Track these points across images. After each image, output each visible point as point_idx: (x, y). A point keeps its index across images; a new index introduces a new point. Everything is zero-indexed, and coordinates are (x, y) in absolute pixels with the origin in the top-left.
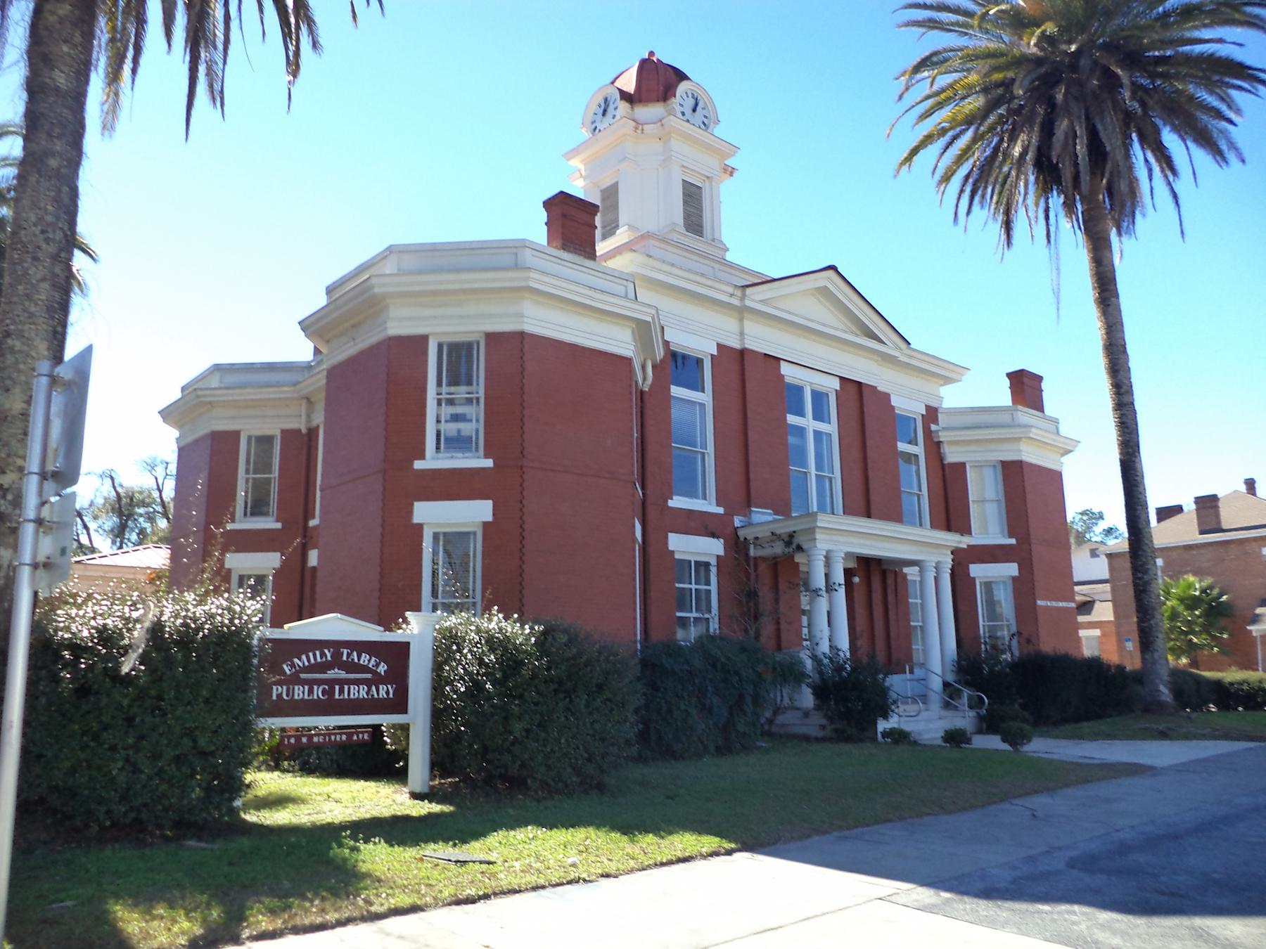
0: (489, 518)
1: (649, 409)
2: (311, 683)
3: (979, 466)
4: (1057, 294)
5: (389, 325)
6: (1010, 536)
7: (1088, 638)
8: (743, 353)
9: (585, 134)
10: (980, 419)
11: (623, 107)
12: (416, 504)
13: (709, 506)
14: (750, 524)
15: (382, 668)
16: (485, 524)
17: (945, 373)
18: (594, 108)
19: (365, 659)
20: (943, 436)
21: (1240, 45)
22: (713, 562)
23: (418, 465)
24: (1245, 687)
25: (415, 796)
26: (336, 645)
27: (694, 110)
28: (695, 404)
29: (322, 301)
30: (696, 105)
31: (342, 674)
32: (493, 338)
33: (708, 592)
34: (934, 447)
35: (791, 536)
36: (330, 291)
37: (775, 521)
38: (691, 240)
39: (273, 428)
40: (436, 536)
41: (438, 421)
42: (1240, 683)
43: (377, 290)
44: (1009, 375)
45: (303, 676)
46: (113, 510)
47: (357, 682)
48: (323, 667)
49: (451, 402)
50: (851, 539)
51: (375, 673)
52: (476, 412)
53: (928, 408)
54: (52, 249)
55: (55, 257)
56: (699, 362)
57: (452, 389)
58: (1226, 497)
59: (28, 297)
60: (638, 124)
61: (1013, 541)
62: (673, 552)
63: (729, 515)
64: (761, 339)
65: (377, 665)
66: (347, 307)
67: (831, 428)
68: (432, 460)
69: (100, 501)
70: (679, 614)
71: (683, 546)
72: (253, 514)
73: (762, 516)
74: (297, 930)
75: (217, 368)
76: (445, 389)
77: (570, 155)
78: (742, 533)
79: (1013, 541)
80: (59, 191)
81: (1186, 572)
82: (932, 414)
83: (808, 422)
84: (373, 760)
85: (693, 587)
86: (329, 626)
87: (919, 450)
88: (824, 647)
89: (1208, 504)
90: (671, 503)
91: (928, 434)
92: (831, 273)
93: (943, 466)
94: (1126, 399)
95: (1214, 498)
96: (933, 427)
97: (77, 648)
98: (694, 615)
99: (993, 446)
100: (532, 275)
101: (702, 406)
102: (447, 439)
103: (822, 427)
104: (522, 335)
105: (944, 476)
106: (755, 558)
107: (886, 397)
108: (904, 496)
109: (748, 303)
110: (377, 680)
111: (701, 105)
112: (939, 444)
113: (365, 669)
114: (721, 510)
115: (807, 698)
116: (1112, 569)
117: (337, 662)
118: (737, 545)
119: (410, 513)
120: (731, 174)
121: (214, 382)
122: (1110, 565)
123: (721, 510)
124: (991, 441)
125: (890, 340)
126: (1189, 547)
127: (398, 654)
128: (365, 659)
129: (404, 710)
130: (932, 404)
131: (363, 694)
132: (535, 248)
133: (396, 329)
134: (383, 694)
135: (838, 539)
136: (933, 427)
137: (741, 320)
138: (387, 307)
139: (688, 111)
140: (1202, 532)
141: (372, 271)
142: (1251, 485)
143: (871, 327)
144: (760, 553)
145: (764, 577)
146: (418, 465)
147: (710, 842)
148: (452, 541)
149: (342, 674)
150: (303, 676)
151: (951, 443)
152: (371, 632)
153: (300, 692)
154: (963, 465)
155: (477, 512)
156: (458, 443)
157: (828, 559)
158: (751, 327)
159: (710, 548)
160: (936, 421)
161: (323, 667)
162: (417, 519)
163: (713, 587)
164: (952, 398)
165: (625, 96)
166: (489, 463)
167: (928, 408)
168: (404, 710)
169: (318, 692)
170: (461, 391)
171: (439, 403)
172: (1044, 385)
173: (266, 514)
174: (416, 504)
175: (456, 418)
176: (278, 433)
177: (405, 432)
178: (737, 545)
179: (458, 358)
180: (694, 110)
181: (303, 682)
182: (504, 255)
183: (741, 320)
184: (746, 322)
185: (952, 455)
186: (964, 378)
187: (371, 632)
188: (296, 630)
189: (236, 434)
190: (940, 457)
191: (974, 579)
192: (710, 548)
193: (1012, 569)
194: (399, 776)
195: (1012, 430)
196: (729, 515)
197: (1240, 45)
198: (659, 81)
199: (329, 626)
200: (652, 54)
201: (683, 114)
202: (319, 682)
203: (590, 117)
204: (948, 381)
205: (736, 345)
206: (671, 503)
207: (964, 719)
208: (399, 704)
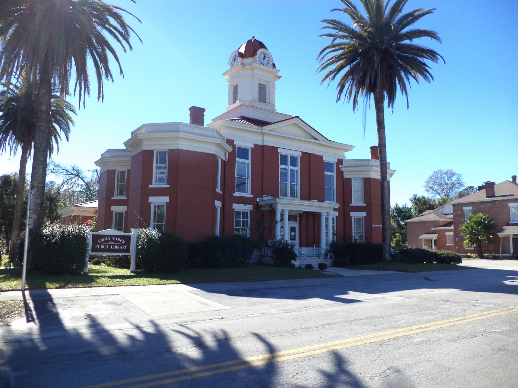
0: (252, 209)
1: (228, 165)
2: (105, 245)
3: (355, 179)
4: (364, 128)
5: (143, 147)
6: (365, 203)
7: (448, 235)
8: (263, 146)
9: (229, 67)
10: (359, 164)
11: (239, 59)
12: (150, 197)
13: (248, 195)
14: (263, 200)
15: (123, 242)
16: (167, 203)
17: (349, 148)
18: (232, 58)
19: (119, 239)
20: (343, 169)
22: (249, 212)
23: (351, 205)
24: (443, 256)
25: (131, 272)
26: (112, 236)
27: (264, 59)
28: (244, 166)
29: (130, 137)
30: (265, 57)
31: (113, 243)
32: (171, 151)
33: (247, 221)
34: (340, 173)
35: (272, 204)
36: (132, 133)
37: (272, 199)
38: (262, 105)
39: (125, 169)
41: (156, 174)
42: (441, 254)
43: (139, 138)
44: (370, 148)
46: (98, 183)
47: (117, 245)
48: (108, 241)
49: (160, 168)
50: (291, 206)
51: (122, 243)
52: (166, 171)
53: (338, 160)
54: (42, 148)
55: (44, 150)
56: (247, 150)
57: (161, 165)
58: (501, 184)
59: (38, 160)
60: (243, 65)
61: (365, 205)
63: (255, 197)
64: (269, 141)
66: (134, 141)
67: (298, 168)
68: (154, 185)
69: (94, 180)
71: (237, 207)
72: (120, 195)
73: (267, 198)
74: (75, 288)
75: (109, 151)
76: (158, 165)
77: (224, 74)
78: (259, 203)
79: (365, 205)
80: (44, 135)
81: (479, 212)
82: (340, 162)
83: (289, 167)
84: (123, 263)
85: (242, 219)
86: (110, 232)
87: (334, 174)
88: (279, 238)
89: (489, 187)
91: (338, 169)
92: (297, 119)
93: (343, 179)
94: (383, 162)
95: (493, 184)
96: (340, 166)
97: (46, 236)
99: (361, 173)
100: (180, 133)
101: (297, 171)
102: (159, 179)
103: (294, 168)
104: (178, 150)
105: (343, 183)
106: (263, 211)
107: (321, 157)
108: (326, 190)
109: (263, 131)
110: (122, 244)
111: (267, 56)
112: (342, 172)
113: (119, 242)
114: (252, 196)
115: (269, 253)
116: (454, 210)
117: (112, 240)
118: (257, 207)
119: (148, 200)
120: (280, 78)
121: (108, 155)
122: (453, 208)
123: (252, 196)
124: (360, 171)
126: (482, 203)
127: (128, 239)
128: (119, 239)
129: (129, 252)
130: (340, 158)
131: (118, 247)
132: (184, 125)
133: (145, 148)
134: (123, 248)
135: (287, 205)
136: (340, 166)
137: (263, 136)
138: (142, 142)
139: (262, 59)
140: (487, 197)
141: (136, 133)
142: (514, 178)
143: (314, 136)
144: (264, 209)
145: (265, 217)
146: (150, 186)
147: (177, 282)
148: (359, 220)
149: (113, 243)
151: (346, 171)
152: (121, 233)
153: (102, 247)
154: (350, 179)
155: (165, 199)
156: (161, 180)
158: (266, 138)
159: (248, 208)
160: (342, 164)
161: (108, 241)
162: (149, 201)
163: (249, 220)
164: (349, 156)
165: (241, 55)
166: (168, 186)
167: (338, 160)
168: (129, 252)
169: (107, 247)
170: (162, 165)
171: (157, 168)
172: (205, 113)
173: (123, 194)
174: (150, 197)
175: (161, 173)
176: (126, 170)
177: (147, 177)
178: (257, 207)
179: (162, 154)
180: (264, 59)
181: (103, 245)
182: (172, 128)
183: (263, 136)
184: (265, 137)
185: (346, 176)
186: (353, 149)
187: (121, 233)
188: (102, 232)
189: (115, 170)
190: (343, 176)
191: (351, 217)
192: (248, 208)
193: (364, 214)
194: (128, 267)
195: (367, 167)
196: (255, 197)
198: (254, 47)
199: (110, 232)
200: (253, 37)
201: (260, 61)
202: (107, 245)
203: (231, 61)
205: (261, 144)
206: (234, 195)
207: (328, 262)
208: (128, 250)
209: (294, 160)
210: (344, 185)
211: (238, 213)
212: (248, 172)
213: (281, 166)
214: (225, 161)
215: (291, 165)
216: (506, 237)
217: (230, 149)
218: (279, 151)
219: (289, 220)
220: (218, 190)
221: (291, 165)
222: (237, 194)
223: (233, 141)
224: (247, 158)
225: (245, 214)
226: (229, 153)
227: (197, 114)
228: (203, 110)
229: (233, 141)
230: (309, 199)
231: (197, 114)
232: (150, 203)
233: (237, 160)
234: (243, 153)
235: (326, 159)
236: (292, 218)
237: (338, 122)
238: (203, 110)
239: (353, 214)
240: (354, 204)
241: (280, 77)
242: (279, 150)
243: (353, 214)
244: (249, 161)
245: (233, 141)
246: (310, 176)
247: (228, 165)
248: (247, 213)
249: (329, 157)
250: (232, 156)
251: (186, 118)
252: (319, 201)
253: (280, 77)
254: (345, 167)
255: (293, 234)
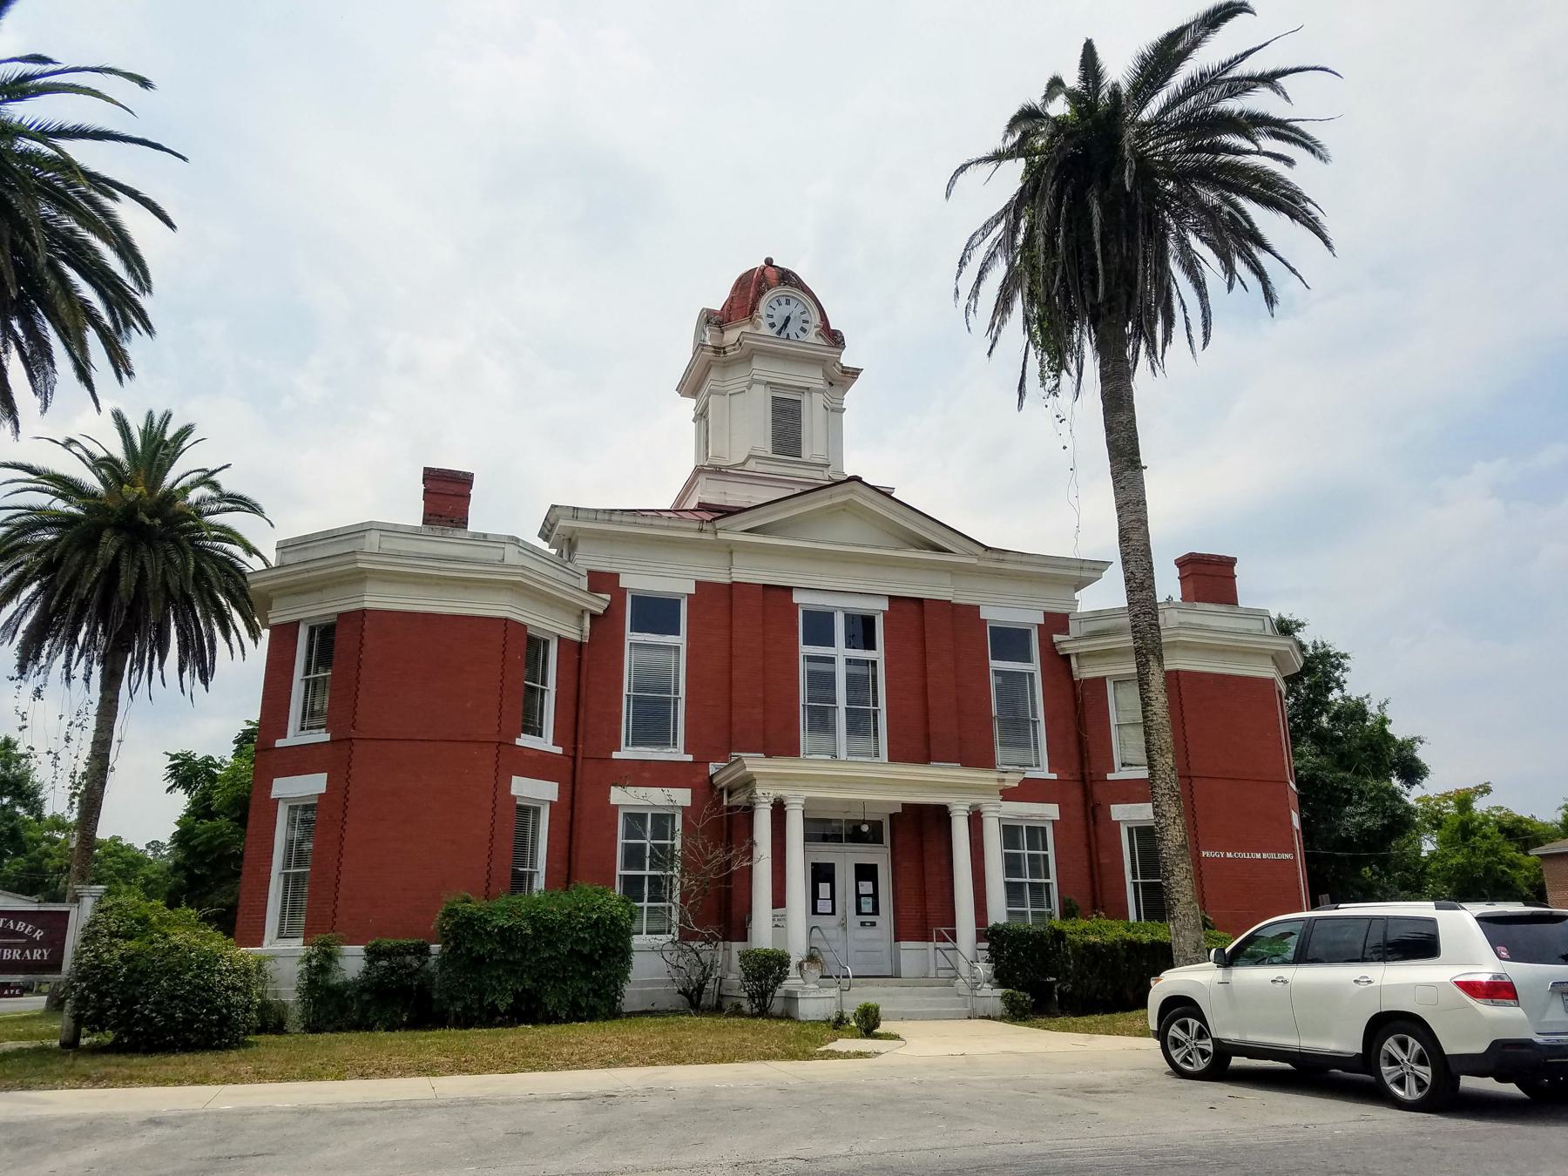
0: (555, 799)
1: (590, 661)
12: (556, 785)
13: (677, 753)
15: (38, 935)
19: (21, 926)
21: (144, 83)
27: (788, 319)
28: (657, 659)
33: (1046, 857)
34: (1058, 664)
40: (1130, 830)
45: (1468, 1083)
56: (1027, 633)
62: (515, 798)
63: (701, 762)
65: (34, 932)
70: (540, 883)
71: (525, 788)
82: (1057, 622)
83: (840, 651)
85: (1026, 852)
87: (1034, 667)
90: (518, 742)
91: (1049, 650)
92: (855, 485)
93: (1074, 684)
98: (647, 872)
110: (32, 944)
113: (21, 935)
114: (690, 758)
118: (708, 791)
123: (690, 758)
125: (953, 544)
128: (21, 926)
131: (16, 955)
134: (37, 956)
136: (1056, 638)
143: (927, 538)
150: (1468, 1083)
155: (313, 785)
157: (779, 810)
160: (1065, 629)
174: (556, 785)
178: (708, 791)
180: (788, 319)
192: (683, 796)
196: (701, 762)
197: (144, 83)
204: (1081, 584)
206: (518, 742)
209: (862, 630)
210: (1078, 708)
211: (636, 820)
212: (677, 676)
213: (805, 650)
214: (581, 644)
215: (849, 645)
216: (813, 872)
217: (599, 603)
218: (795, 600)
219: (808, 838)
220: (545, 743)
221: (849, 645)
222: (626, 753)
223: (617, 576)
224: (1028, 660)
225: (662, 822)
226: (594, 616)
227: (447, 494)
228: (1231, 562)
229: (617, 576)
230: (926, 757)
231: (447, 494)
232: (276, 801)
233: (631, 637)
234: (656, 613)
235: (995, 613)
236: (821, 830)
237: (973, 446)
238: (1231, 562)
239: (618, 796)
240: (1119, 774)
241: (854, 373)
242: (797, 598)
243: (1120, 812)
244: (681, 640)
245: (615, 577)
246: (925, 676)
247: (590, 661)
248: (1044, 829)
249: (1004, 609)
250: (605, 625)
251: (411, 511)
252: (966, 763)
253: (854, 373)
254: (1076, 639)
255: (866, 887)
